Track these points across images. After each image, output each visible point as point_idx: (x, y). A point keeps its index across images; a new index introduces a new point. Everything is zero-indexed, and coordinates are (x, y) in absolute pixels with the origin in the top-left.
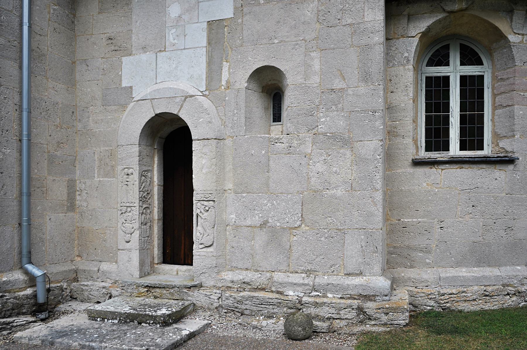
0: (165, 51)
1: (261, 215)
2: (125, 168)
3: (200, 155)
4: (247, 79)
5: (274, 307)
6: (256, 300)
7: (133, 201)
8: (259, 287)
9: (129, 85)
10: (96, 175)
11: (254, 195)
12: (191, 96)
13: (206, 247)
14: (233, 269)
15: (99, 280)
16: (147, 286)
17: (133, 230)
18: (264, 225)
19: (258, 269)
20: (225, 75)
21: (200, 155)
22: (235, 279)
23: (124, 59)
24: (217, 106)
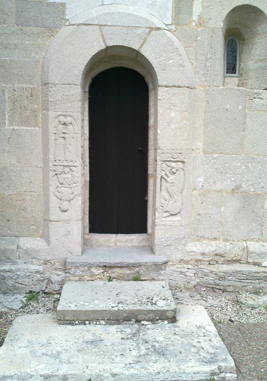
1: (233, 179)
2: (59, 116)
3: (167, 106)
5: (260, 281)
6: (240, 275)
7: (74, 159)
8: (234, 259)
10: (7, 122)
11: (227, 156)
12: (158, 29)
13: (172, 215)
14: (200, 238)
17: (72, 196)
18: (236, 191)
19: (228, 238)
21: (167, 106)
22: (207, 251)
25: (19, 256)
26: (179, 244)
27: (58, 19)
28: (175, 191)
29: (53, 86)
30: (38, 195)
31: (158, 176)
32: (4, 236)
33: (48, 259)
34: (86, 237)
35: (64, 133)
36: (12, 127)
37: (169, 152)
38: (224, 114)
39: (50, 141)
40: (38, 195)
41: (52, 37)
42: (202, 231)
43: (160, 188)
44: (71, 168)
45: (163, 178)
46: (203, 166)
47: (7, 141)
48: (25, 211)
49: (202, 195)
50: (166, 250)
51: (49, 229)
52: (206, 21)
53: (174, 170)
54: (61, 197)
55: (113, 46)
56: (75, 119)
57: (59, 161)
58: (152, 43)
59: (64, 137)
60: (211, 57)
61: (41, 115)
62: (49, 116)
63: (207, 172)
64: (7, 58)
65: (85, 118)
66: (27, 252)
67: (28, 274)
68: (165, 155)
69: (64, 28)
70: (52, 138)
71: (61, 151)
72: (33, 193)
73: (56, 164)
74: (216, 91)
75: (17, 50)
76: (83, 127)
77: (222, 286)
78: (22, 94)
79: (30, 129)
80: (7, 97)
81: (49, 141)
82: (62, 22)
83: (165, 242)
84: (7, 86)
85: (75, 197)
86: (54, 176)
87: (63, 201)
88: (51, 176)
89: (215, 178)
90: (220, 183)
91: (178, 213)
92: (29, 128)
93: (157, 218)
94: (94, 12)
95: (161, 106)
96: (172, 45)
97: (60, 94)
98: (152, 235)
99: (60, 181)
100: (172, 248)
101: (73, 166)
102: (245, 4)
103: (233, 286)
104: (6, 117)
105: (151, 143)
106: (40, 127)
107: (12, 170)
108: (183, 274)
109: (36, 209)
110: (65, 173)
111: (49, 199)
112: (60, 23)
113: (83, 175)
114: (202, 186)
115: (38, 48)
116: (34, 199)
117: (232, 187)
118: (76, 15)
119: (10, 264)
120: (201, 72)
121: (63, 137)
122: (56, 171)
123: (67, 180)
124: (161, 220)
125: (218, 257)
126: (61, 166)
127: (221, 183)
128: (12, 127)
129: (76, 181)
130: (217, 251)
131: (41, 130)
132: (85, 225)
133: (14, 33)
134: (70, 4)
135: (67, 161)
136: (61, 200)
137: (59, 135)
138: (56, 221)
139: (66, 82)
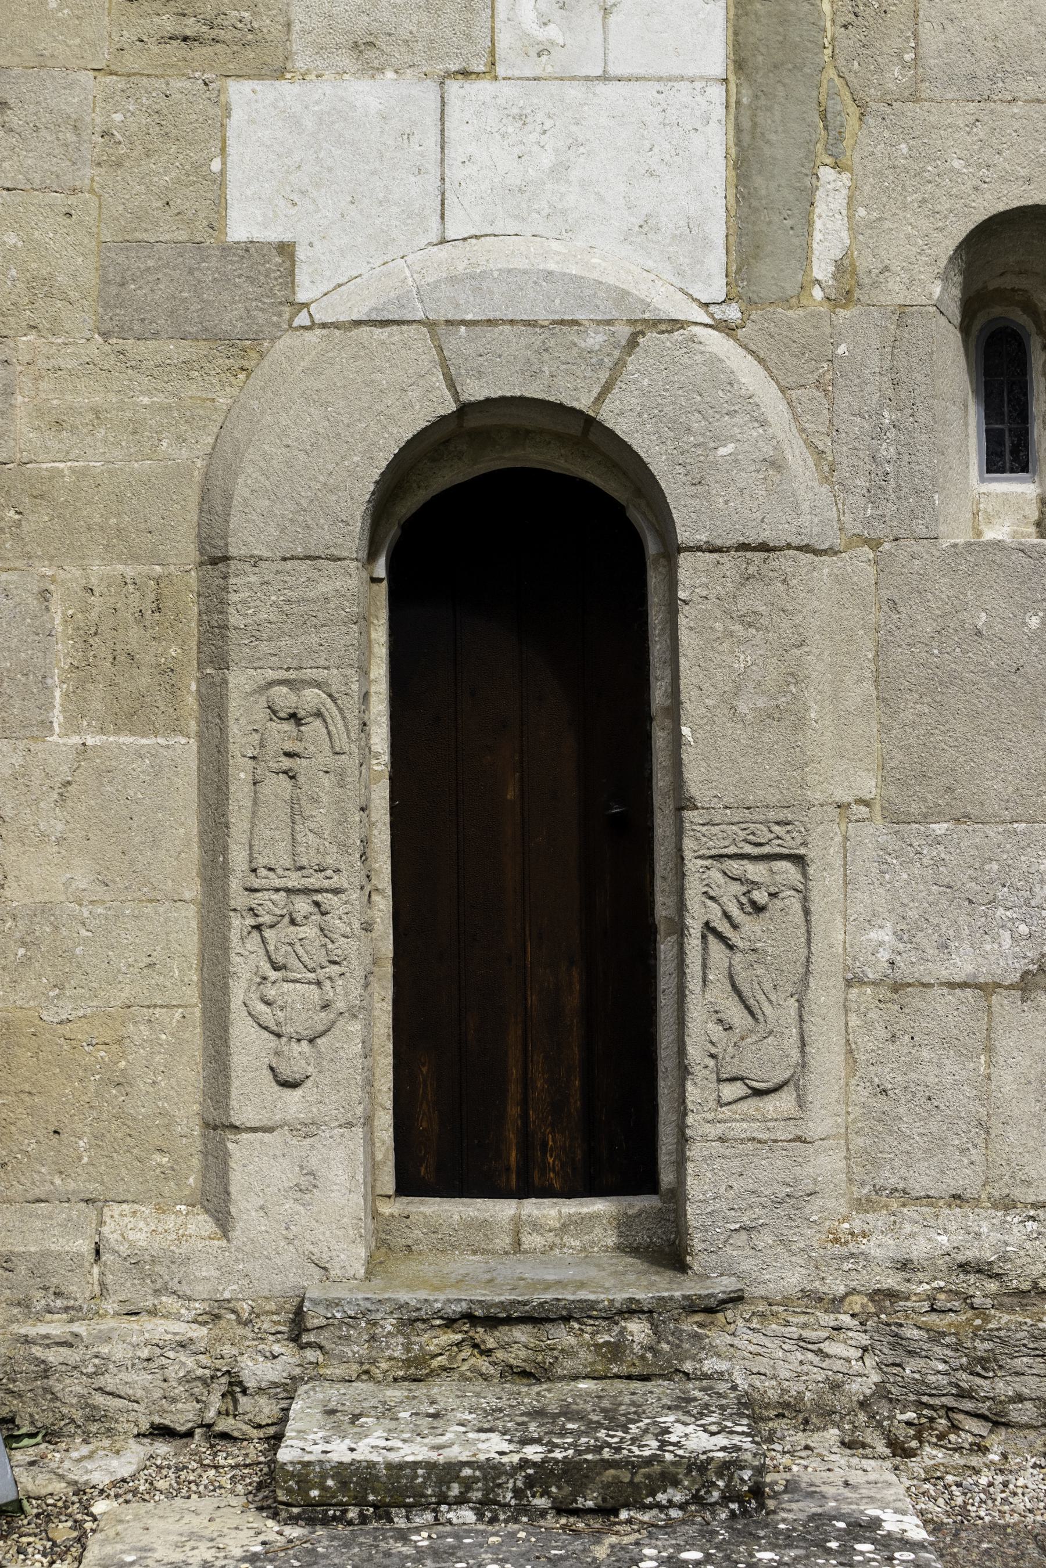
0: (491, 72)
1: (1023, 929)
2: (271, 684)
4: (943, 262)
7: (330, 860)
9: (274, 235)
10: (57, 717)
11: (990, 830)
13: (758, 1093)
15: (110, 1306)
16: (469, 1317)
17: (323, 1018)
19: (1018, 1193)
20: (829, 237)
22: (919, 1249)
23: (239, 92)
24: (791, 381)
25: (102, 1284)
26: (793, 1224)
27: (264, 303)
28: (768, 986)
29: (248, 568)
30: (178, 1021)
31: (689, 921)
32: (39, 1201)
33: (227, 1295)
34: (387, 1208)
35: (288, 755)
36: (76, 740)
37: (735, 820)
38: (965, 652)
39: (232, 789)
40: (178, 1021)
41: (242, 376)
42: (897, 1163)
43: (700, 973)
44: (318, 898)
45: (714, 931)
46: (887, 876)
47: (56, 796)
48: (129, 1089)
49: (889, 1005)
50: (735, 1253)
51: (226, 1163)
52: (867, 280)
53: (760, 897)
54: (278, 1024)
55: (488, 401)
56: (336, 695)
57: (270, 869)
58: (646, 382)
59: (291, 769)
60: (897, 423)
61: (194, 687)
62: (230, 685)
63: (905, 901)
64: (61, 465)
65: (373, 689)
66: (137, 1264)
67: (145, 1353)
68: (715, 830)
69: (286, 341)
70: (242, 775)
71: (277, 828)
72: (158, 1009)
73: (256, 886)
74: (926, 556)
75: (103, 431)
76: (365, 724)
77: (988, 1398)
78: (119, 605)
79: (148, 742)
80: (58, 620)
81: (228, 788)
82: (280, 315)
83: (733, 1213)
84: (62, 575)
85: (334, 1023)
86: (250, 933)
87: (284, 1040)
88: (234, 935)
89: (943, 927)
90: (966, 945)
91: (785, 1083)
92: (144, 741)
93: (690, 1106)
94: (408, 273)
95: (691, 629)
96: (730, 384)
97: (273, 598)
98: (677, 1197)
99: (273, 957)
100: (766, 1239)
101: (327, 891)
102: (1030, 202)
103: (1038, 1399)
104: (53, 698)
105: (661, 783)
106: (192, 735)
107: (75, 917)
108: (809, 1346)
109: (173, 1081)
110: (293, 922)
111: (227, 1031)
112: (275, 319)
113: (368, 927)
114: (886, 965)
115: (186, 421)
116: (164, 1037)
117: (1021, 965)
118: (340, 285)
119: (64, 1316)
120: (858, 482)
121: (285, 772)
122: (257, 916)
123: (301, 951)
124: (710, 1116)
125: (972, 1278)
126: (277, 890)
127: (972, 946)
128: (76, 740)
129: (340, 952)
130: (967, 1252)
131: (194, 747)
132: (379, 1157)
133: (91, 366)
134: (311, 245)
135: (302, 868)
136: (279, 1036)
137: (271, 764)
138: (254, 1130)
139: (300, 551)
